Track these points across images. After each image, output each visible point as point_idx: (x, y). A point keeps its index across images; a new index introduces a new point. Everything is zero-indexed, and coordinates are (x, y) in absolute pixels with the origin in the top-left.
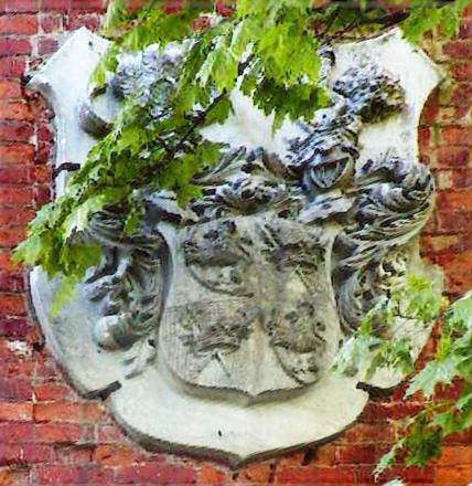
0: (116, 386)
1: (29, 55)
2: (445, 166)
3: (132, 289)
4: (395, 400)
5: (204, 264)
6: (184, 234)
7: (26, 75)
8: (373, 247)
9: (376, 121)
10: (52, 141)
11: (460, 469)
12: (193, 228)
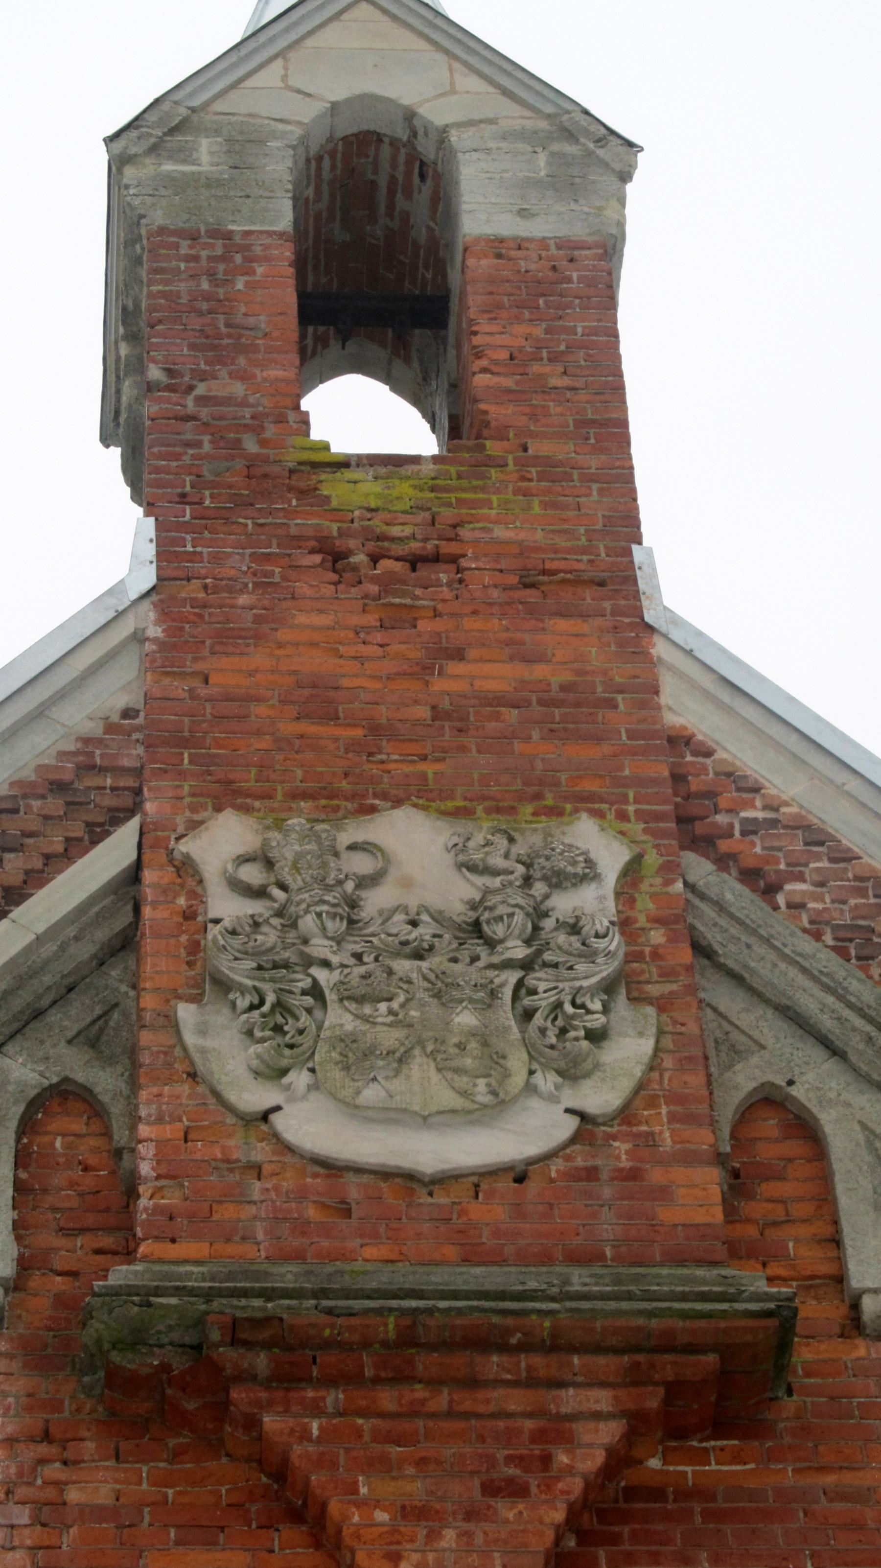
0: (278, 1108)
1: (175, 830)
2: (656, 925)
3: (287, 1024)
4: (619, 1125)
5: (360, 1000)
6: (336, 976)
7: (171, 847)
8: (555, 988)
9: (566, 888)
10: (202, 902)
11: (704, 1189)
12: (346, 971)
